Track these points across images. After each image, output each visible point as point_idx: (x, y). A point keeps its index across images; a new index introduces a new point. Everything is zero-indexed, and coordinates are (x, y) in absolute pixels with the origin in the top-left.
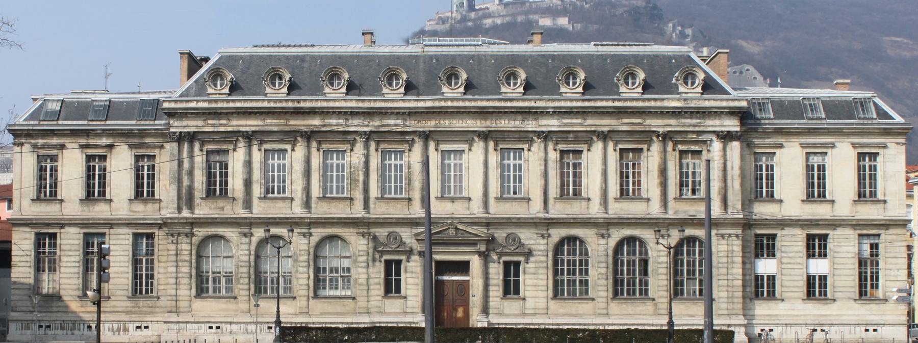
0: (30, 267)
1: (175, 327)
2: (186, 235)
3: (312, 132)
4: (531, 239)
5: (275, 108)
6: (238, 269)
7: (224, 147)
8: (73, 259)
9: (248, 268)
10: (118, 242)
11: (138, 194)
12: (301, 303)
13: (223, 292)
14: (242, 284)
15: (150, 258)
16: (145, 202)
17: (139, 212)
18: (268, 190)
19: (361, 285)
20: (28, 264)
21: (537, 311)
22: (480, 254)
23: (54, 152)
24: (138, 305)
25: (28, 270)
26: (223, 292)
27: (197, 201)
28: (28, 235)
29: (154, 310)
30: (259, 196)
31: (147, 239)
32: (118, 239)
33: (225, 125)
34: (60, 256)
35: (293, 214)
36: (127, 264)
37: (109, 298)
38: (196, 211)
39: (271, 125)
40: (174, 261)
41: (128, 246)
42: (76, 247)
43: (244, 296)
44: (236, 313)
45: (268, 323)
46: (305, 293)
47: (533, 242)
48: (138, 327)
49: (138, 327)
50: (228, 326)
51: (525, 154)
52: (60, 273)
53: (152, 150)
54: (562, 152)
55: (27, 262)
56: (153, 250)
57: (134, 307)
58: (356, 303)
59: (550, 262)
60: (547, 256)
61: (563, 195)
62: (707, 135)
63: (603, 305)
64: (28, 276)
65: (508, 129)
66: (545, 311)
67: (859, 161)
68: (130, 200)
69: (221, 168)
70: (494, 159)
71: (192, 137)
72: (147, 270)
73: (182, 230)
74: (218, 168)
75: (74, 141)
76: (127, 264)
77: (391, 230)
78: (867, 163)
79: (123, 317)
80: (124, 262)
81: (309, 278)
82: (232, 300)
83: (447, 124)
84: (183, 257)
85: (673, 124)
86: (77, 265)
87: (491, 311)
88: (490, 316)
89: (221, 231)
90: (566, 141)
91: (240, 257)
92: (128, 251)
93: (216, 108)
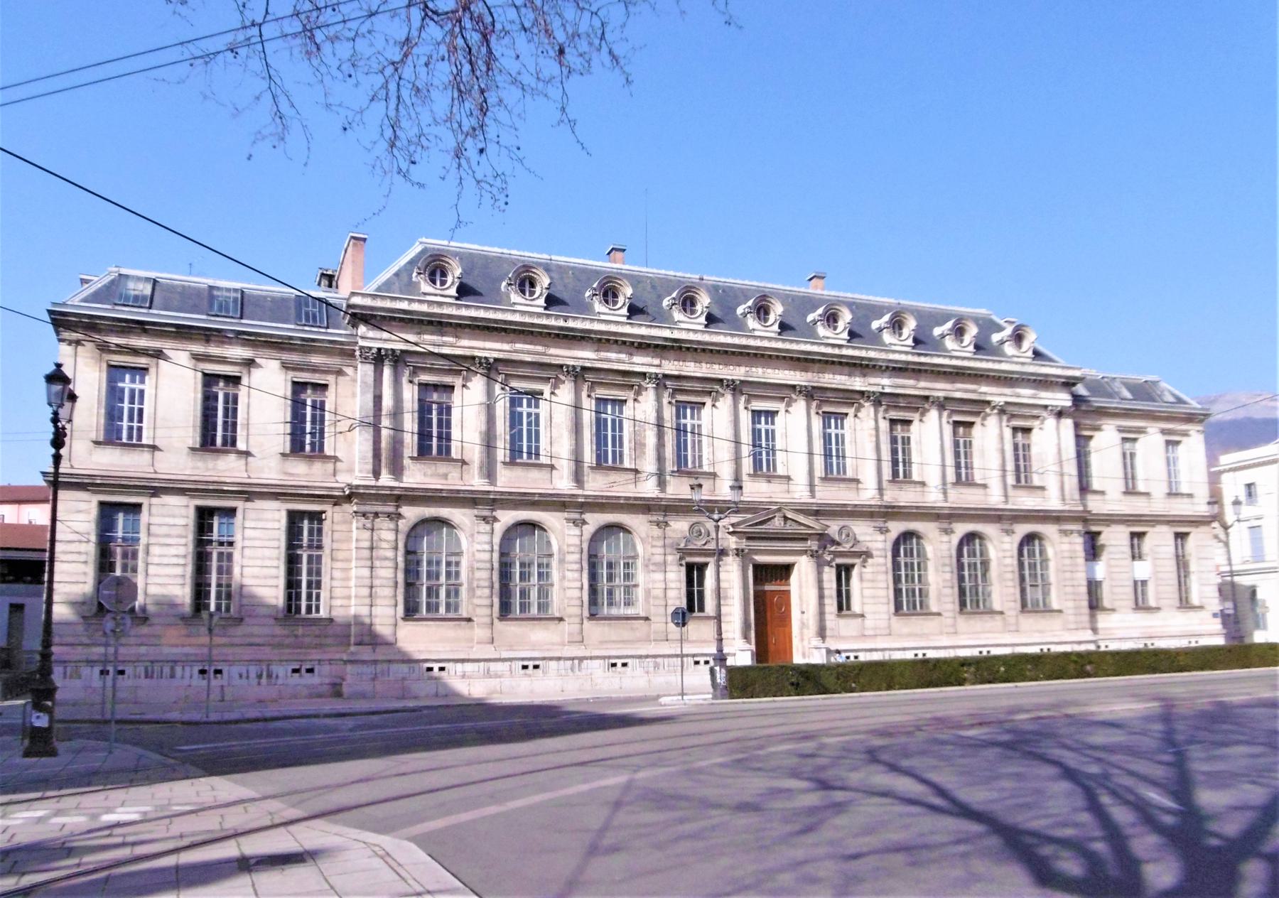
0: (85, 562)
1: (368, 670)
2: (389, 515)
3: (584, 369)
4: (866, 534)
5: (533, 325)
6: (473, 574)
7: (448, 380)
8: (173, 551)
9: (489, 572)
10: (260, 525)
11: (297, 447)
12: (569, 627)
13: (442, 610)
14: (480, 597)
15: (315, 553)
16: (310, 458)
17: (298, 475)
18: (515, 451)
19: (656, 598)
20: (83, 558)
21: (878, 632)
22: (814, 555)
23: (142, 361)
24: (296, 633)
25: (82, 568)
26: (442, 610)
27: (407, 462)
28: (83, 506)
29: (324, 641)
30: (502, 459)
31: (311, 521)
32: (259, 520)
33: (452, 346)
34: (148, 546)
35: (156, 472)
36: (275, 563)
37: (242, 620)
38: (405, 479)
39: (522, 352)
40: (367, 559)
41: (278, 532)
42: (180, 531)
43: (482, 616)
44: (470, 645)
45: (523, 659)
46: (577, 611)
47: (868, 538)
48: (295, 671)
49: (295, 671)
50: (459, 666)
51: (848, 422)
52: (147, 574)
53: (323, 376)
54: (424, 387)
55: (79, 553)
56: (320, 541)
57: (288, 636)
58: (650, 625)
59: (890, 565)
60: (886, 557)
61: (600, 465)
62: (635, 377)
63: (950, 621)
64: (82, 579)
65: (833, 386)
66: (888, 631)
67: (753, 423)
68: (283, 455)
69: (440, 413)
70: (817, 423)
71: (398, 359)
72: (310, 573)
73: (380, 509)
74: (434, 413)
75: (180, 346)
76: (275, 563)
77: (695, 520)
78: (763, 426)
79: (267, 653)
80: (270, 559)
81: (582, 588)
82: (463, 623)
83: (761, 373)
84: (382, 553)
85: (885, 383)
86: (182, 561)
87: (828, 633)
88: (827, 639)
89: (444, 512)
90: (896, 407)
91: (476, 554)
92: (279, 540)
93: (442, 315)
